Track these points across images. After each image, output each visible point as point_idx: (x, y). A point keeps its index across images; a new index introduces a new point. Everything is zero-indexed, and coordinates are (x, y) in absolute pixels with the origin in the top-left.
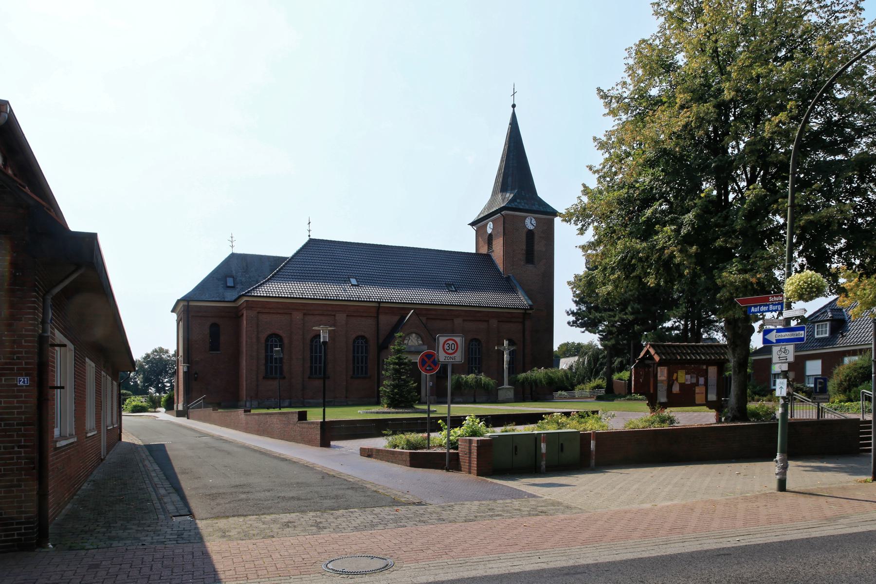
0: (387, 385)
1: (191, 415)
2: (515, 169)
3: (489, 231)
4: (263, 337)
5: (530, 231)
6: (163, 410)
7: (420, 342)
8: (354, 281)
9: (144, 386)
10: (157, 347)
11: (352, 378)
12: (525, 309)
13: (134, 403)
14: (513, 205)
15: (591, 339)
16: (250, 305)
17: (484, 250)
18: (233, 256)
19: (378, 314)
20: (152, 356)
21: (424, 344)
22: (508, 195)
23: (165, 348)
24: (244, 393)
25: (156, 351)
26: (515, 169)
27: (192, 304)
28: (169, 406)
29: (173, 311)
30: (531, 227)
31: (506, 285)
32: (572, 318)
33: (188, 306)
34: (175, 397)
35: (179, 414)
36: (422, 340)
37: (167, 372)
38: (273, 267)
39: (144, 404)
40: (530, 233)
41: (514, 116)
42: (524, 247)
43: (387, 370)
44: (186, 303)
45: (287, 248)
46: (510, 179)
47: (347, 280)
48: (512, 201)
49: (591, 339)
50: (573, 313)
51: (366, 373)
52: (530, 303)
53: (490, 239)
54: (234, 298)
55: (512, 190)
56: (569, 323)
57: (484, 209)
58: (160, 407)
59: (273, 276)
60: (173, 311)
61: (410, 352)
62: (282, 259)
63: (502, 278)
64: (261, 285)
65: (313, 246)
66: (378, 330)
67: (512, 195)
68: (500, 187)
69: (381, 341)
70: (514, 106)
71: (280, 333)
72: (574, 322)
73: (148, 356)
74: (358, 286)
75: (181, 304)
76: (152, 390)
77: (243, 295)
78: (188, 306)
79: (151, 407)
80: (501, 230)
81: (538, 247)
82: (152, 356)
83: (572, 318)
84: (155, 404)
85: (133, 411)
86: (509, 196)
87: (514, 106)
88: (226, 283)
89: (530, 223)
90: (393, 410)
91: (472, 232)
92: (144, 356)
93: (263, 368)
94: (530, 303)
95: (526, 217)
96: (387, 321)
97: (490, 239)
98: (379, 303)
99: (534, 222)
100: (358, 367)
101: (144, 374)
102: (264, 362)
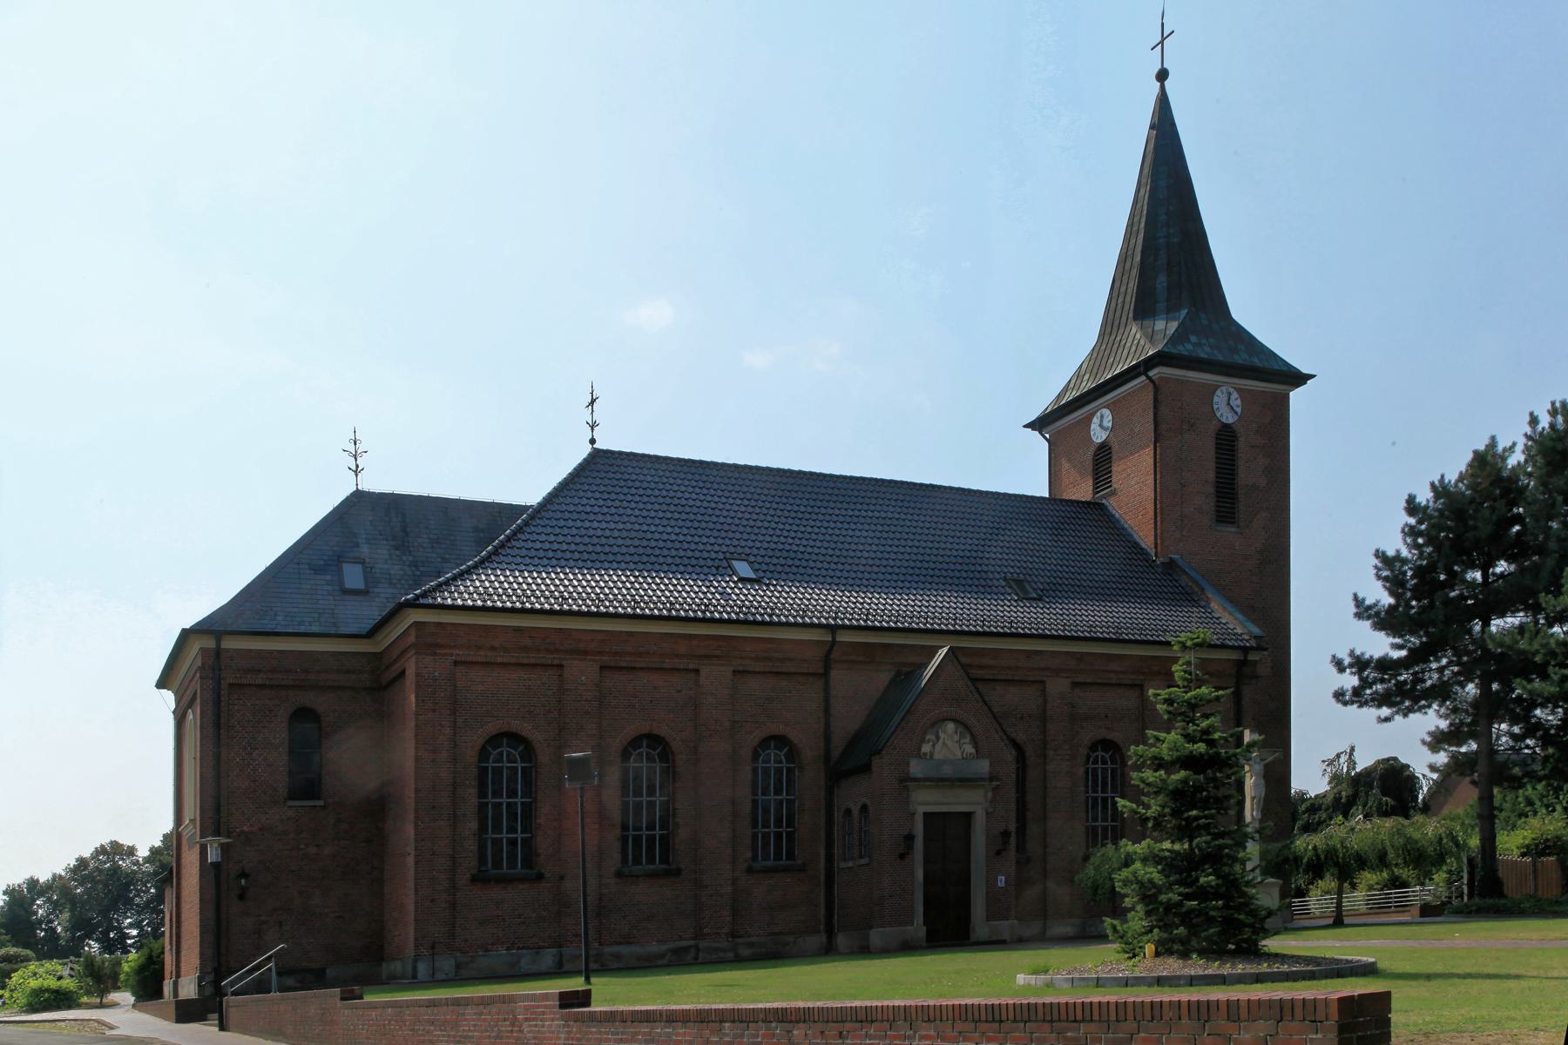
0: (1138, 860)
1: (233, 1015)
2: (1168, 252)
3: (1098, 435)
4: (474, 739)
5: (1226, 427)
6: (125, 997)
7: (970, 749)
8: (743, 569)
9: (73, 938)
10: (105, 840)
11: (750, 870)
12: (1245, 650)
13: (34, 984)
14: (1184, 349)
15: (1411, 740)
16: (429, 640)
17: (1083, 491)
18: (359, 499)
19: (827, 662)
20: (92, 865)
21: (979, 753)
22: (1160, 325)
23: (126, 841)
24: (405, 934)
25: (101, 850)
26: (1168, 252)
27: (230, 644)
28: (149, 986)
29: (161, 684)
30: (1229, 418)
31: (1166, 580)
32: (1350, 681)
33: (218, 652)
34: (169, 959)
35: (187, 1013)
36: (975, 742)
37: (129, 901)
38: (488, 530)
39: (69, 984)
40: (1226, 438)
41: (1163, 103)
42: (1211, 476)
43: (1135, 795)
44: (210, 643)
45: (528, 486)
46: (1162, 281)
47: (722, 567)
48: (1175, 339)
49: (1411, 740)
50: (1360, 664)
51: (790, 855)
52: (1256, 630)
53: (1103, 458)
54: (366, 626)
55: (1170, 311)
56: (1339, 695)
57: (1079, 374)
58: (117, 988)
59: (496, 552)
60: (161, 684)
61: (940, 782)
62: (512, 511)
63: (1151, 564)
64: (461, 576)
65: (602, 469)
66: (827, 710)
67: (1174, 325)
68: (1130, 306)
69: (836, 754)
70: (1162, 75)
71: (525, 729)
72: (1357, 692)
73: (82, 863)
74: (758, 581)
75: (195, 648)
76: (93, 947)
77: (412, 604)
78: (218, 652)
79: (89, 993)
80: (1146, 425)
81: (1248, 472)
82: (92, 865)
83: (1350, 681)
84: (101, 981)
85: (32, 1009)
86: (1166, 327)
87: (1162, 75)
88: (341, 582)
89: (1227, 403)
90: (1214, 968)
91: (1038, 446)
92: (73, 863)
93: (471, 845)
94: (1256, 630)
95: (1213, 389)
96: (856, 691)
97: (1103, 458)
98: (833, 629)
99: (1236, 401)
100: (766, 836)
101: (72, 911)
102: (474, 825)
